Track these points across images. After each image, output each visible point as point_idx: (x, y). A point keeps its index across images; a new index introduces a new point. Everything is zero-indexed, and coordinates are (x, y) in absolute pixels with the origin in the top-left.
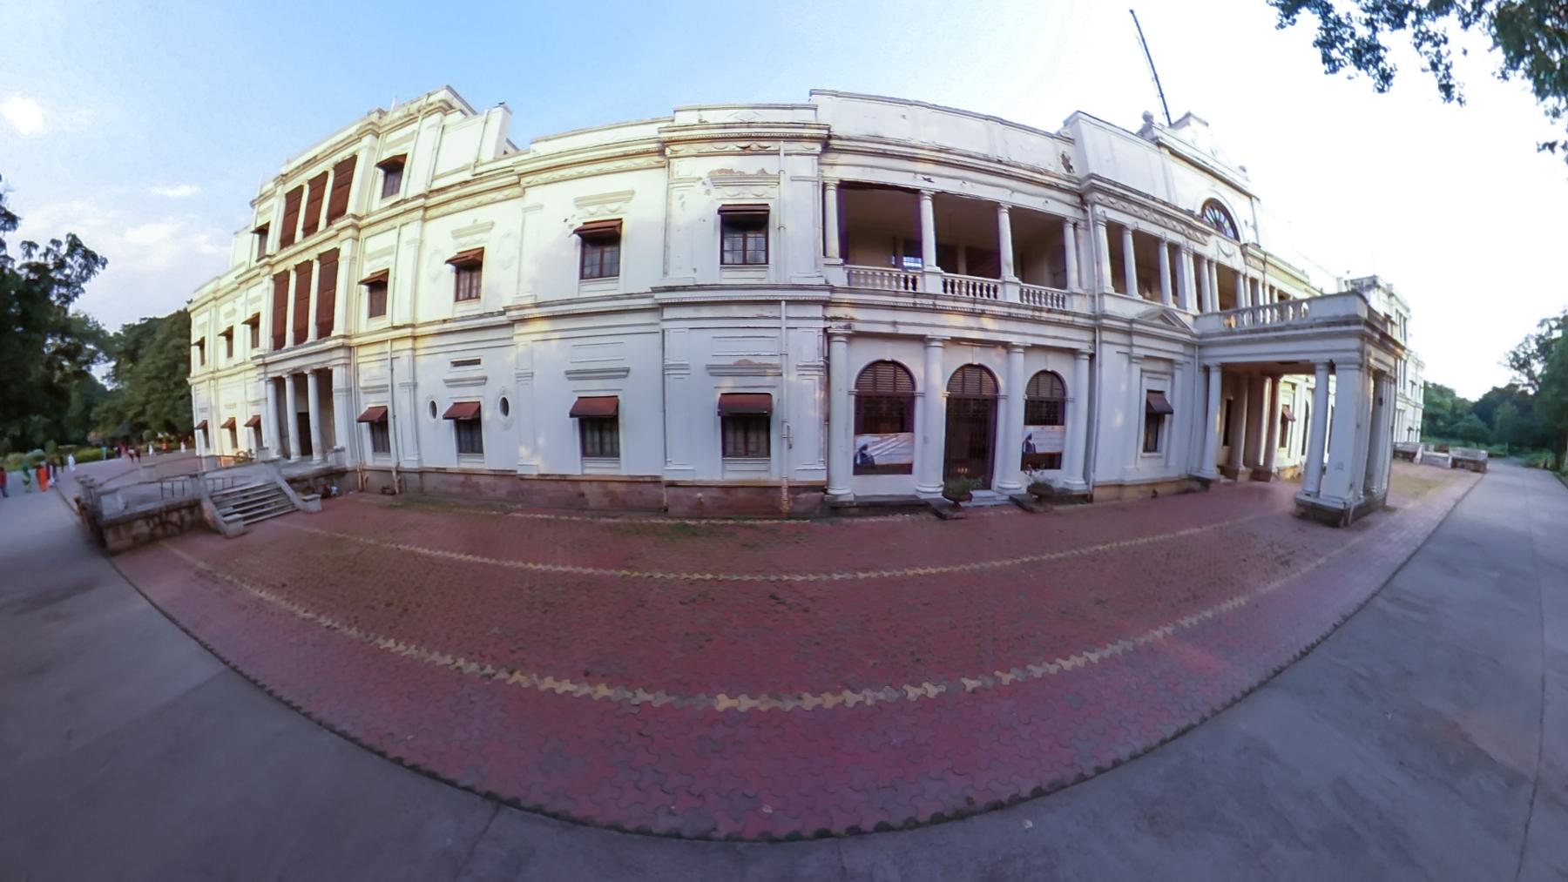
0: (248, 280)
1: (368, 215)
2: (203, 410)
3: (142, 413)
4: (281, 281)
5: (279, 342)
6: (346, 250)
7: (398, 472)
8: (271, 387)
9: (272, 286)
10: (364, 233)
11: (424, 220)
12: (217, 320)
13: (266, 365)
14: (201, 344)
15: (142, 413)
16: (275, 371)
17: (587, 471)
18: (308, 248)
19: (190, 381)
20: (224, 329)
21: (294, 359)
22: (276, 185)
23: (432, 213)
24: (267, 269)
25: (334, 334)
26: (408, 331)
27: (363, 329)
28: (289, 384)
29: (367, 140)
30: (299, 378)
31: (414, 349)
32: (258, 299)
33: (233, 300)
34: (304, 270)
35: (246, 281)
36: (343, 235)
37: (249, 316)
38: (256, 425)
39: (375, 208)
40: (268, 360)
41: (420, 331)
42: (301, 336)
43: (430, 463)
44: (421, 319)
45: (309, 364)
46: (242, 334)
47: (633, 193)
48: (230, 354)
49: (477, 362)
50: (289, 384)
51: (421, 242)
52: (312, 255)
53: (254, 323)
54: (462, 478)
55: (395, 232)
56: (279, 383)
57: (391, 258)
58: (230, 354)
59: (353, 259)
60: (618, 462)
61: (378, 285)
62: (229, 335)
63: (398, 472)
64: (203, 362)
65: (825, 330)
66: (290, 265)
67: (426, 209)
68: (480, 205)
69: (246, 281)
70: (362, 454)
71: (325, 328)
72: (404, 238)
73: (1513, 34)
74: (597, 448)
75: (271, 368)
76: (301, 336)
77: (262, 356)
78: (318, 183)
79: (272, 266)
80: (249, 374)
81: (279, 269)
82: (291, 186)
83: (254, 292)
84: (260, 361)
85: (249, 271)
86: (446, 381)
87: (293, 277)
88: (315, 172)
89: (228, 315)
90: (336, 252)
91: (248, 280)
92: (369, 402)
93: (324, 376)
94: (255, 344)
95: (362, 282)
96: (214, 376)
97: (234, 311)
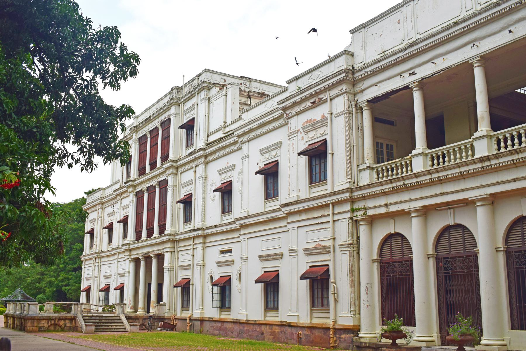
0: (121, 194)
1: (179, 160)
2: (89, 279)
3: (40, 281)
4: (139, 196)
5: (138, 236)
6: (170, 182)
7: (191, 320)
8: (132, 265)
9: (135, 199)
10: (180, 170)
11: (207, 163)
12: (102, 217)
13: (130, 250)
14: (92, 233)
15: (40, 281)
16: (135, 254)
17: (268, 319)
18: (152, 178)
19: (82, 258)
20: (106, 224)
21: (147, 247)
22: (132, 132)
23: (210, 158)
24: (131, 189)
25: (166, 232)
26: (199, 233)
27: (181, 231)
28: (142, 263)
29: (173, 110)
30: (148, 259)
31: (204, 243)
32: (126, 207)
33: (113, 205)
34: (151, 190)
35: (119, 194)
36: (168, 172)
37: (122, 217)
38: (121, 289)
39: (184, 155)
40: (132, 247)
41: (208, 232)
42: (150, 234)
43: (207, 315)
44: (209, 224)
45: (154, 251)
46: (118, 228)
47: (281, 143)
48: (110, 241)
49: (230, 251)
50: (142, 263)
51: (206, 177)
52: (154, 182)
53: (125, 221)
54: (219, 325)
55: (192, 171)
56: (137, 261)
57: (192, 186)
58: (110, 241)
59: (175, 186)
60: (277, 312)
61: (187, 202)
62: (110, 228)
63: (191, 320)
64: (92, 245)
65: (352, 219)
66: (144, 187)
67: (206, 157)
68: (228, 154)
69: (119, 194)
70: (176, 310)
71: (162, 228)
72: (198, 175)
73: (420, 348)
74: (321, 304)
75: (133, 252)
76: (150, 234)
77: (129, 245)
78: (154, 132)
79: (135, 187)
80: (121, 256)
81: (138, 189)
82: (140, 134)
83: (125, 202)
84: (126, 247)
85: (121, 188)
86: (217, 263)
87: (146, 195)
88: (151, 126)
89: (110, 215)
90: (166, 181)
91: (121, 194)
92: (182, 275)
93: (160, 257)
94: (125, 236)
95: (178, 202)
96: (99, 256)
97: (113, 213)
